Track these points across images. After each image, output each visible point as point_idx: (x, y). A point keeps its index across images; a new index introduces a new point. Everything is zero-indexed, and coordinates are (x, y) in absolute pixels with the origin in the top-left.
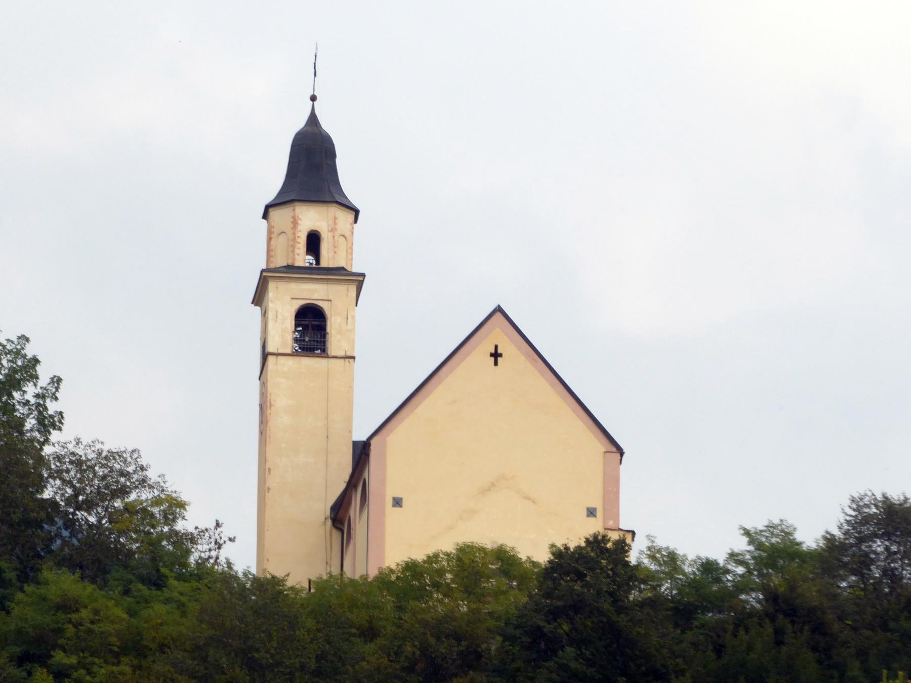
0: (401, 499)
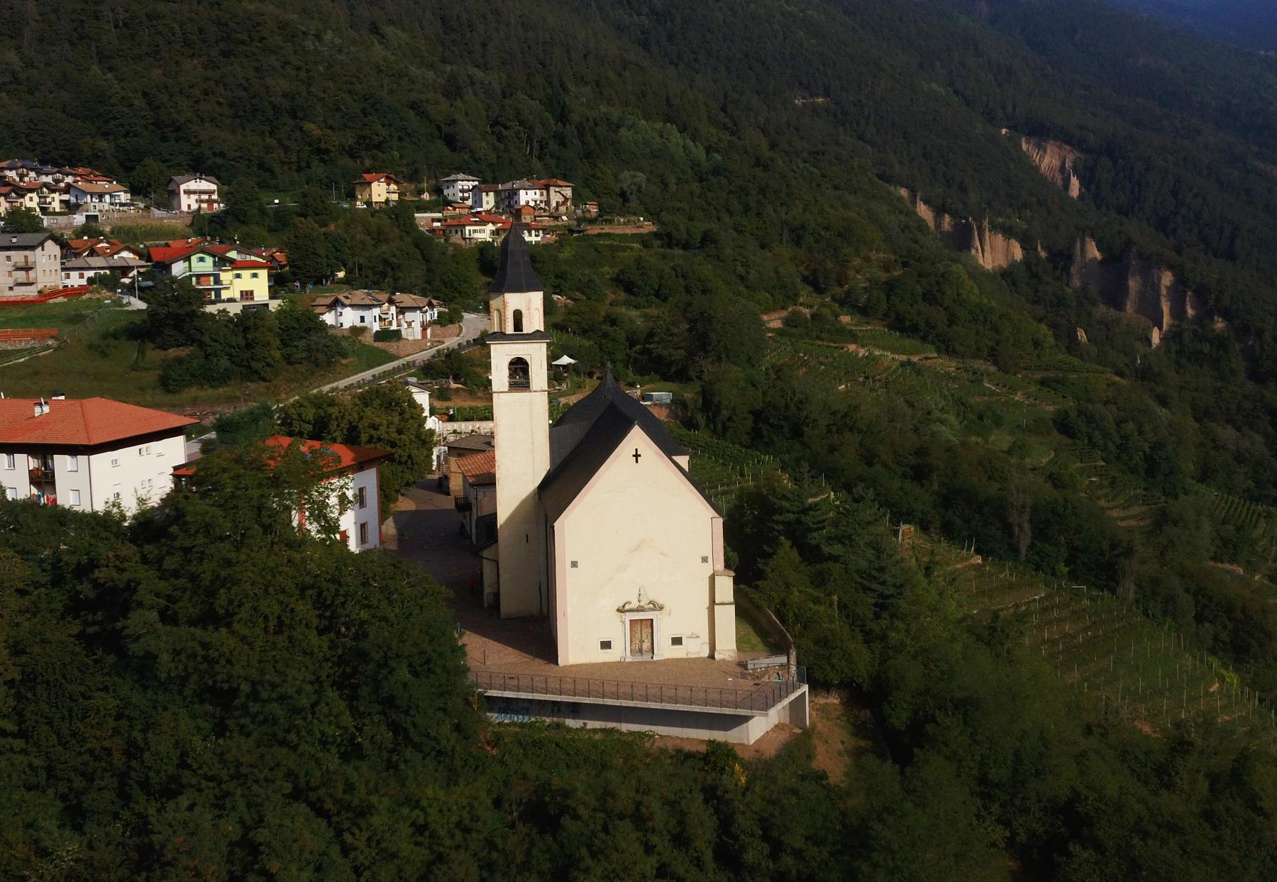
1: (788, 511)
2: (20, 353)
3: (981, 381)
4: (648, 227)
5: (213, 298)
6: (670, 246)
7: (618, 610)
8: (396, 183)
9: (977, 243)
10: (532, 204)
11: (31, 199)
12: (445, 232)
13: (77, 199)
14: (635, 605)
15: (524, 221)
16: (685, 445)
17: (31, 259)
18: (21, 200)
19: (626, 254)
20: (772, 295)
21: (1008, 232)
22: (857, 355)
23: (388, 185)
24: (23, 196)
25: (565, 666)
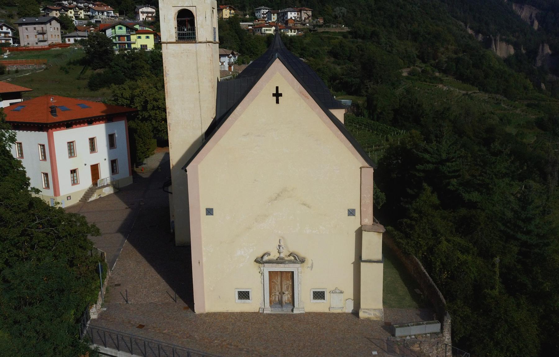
0: (212, 209)
1: (428, 162)
2: (27, 71)
3: (501, 103)
4: (345, 29)
5: (127, 47)
6: (356, 38)
7: (256, 261)
8: (234, 10)
9: (494, 46)
10: (293, 18)
11: (71, 13)
12: (253, 31)
13: (92, 14)
14: (274, 255)
15: (289, 25)
16: (355, 124)
17: (44, 29)
18: (66, 13)
19: (335, 41)
20: (403, 61)
21: (508, 42)
22: (443, 89)
23: (230, 10)
24: (67, 11)
25: (201, 314)
